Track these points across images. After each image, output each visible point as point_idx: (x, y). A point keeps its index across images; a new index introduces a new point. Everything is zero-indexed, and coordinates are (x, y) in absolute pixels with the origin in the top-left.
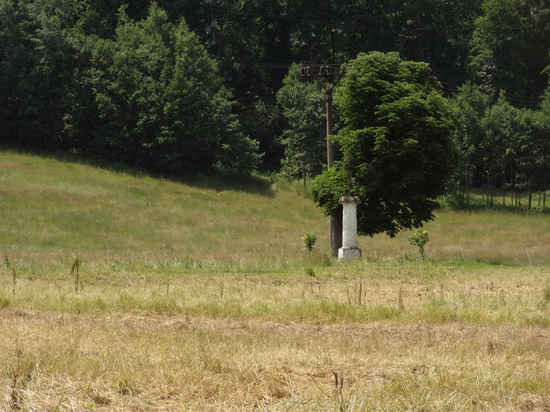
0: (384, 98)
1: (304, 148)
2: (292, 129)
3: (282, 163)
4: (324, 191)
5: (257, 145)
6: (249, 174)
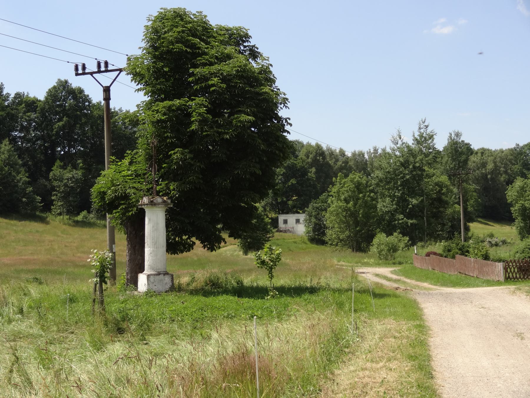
1: (63, 201)
2: (57, 191)
4: (116, 191)
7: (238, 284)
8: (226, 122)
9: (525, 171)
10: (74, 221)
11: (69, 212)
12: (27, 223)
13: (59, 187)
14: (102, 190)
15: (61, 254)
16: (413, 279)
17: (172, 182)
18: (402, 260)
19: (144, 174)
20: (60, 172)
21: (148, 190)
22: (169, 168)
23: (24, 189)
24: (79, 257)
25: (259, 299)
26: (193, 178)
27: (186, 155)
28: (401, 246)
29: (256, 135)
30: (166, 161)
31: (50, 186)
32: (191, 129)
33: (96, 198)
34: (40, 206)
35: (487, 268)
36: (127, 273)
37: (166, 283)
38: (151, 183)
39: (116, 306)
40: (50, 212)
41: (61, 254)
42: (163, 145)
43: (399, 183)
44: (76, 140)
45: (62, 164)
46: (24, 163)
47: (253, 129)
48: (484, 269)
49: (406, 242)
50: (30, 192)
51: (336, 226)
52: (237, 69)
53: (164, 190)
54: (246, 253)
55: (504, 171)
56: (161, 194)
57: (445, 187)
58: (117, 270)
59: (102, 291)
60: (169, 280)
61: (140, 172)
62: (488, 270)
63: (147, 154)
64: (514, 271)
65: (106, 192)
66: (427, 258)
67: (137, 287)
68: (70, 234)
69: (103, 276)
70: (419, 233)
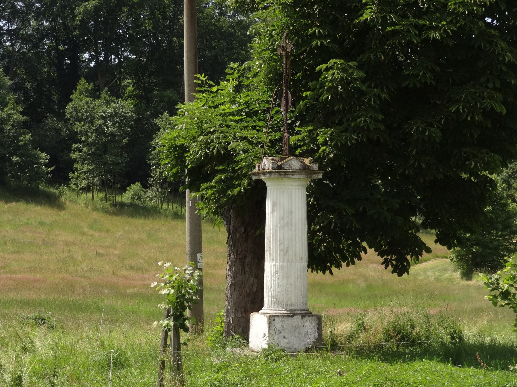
1: (93, 162)
2: (80, 143)
3: (70, 177)
4: (207, 145)
5: (47, 159)
6: (38, 187)
7: (453, 338)
8: (434, 6)
10: (115, 205)
11: (104, 186)
12: (20, 206)
13: (85, 133)
14: (179, 142)
15: (90, 270)
17: (321, 128)
19: (265, 112)
20: (87, 103)
21: (273, 143)
22: (316, 98)
23: (16, 138)
24: (126, 278)
25: (496, 369)
26: (365, 121)
27: (352, 73)
29: (497, 33)
30: (310, 84)
31: (68, 133)
32: (362, 19)
33: (167, 158)
34: (48, 173)
36: (227, 312)
37: (306, 334)
38: (279, 130)
39: (204, 377)
40: (68, 185)
41: (90, 270)
42: (305, 51)
44: (120, 39)
45: (91, 87)
46: (16, 84)
47: (488, 20)
50: (26, 145)
53: (305, 144)
54: (468, 275)
56: (298, 151)
58: (204, 305)
59: (178, 346)
61: (256, 107)
63: (272, 70)
65: (187, 147)
67: (247, 338)
68: (107, 231)
69: (182, 315)
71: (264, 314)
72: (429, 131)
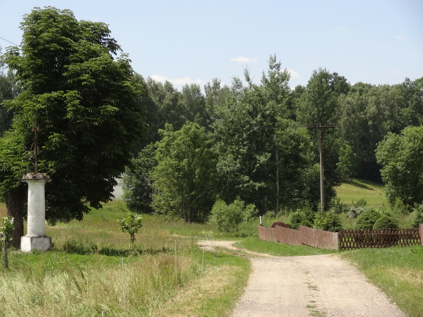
0: (73, 57)
9: (418, 116)
16: (255, 251)
18: (246, 232)
28: (247, 216)
35: (326, 238)
37: (46, 245)
43: (245, 136)
48: (324, 239)
49: (252, 210)
51: (165, 189)
52: (103, 66)
55: (389, 115)
57: (303, 141)
60: (48, 241)
62: (327, 240)
64: (352, 241)
66: (272, 229)
70: (268, 199)
71: (29, 237)
72: (93, 162)
